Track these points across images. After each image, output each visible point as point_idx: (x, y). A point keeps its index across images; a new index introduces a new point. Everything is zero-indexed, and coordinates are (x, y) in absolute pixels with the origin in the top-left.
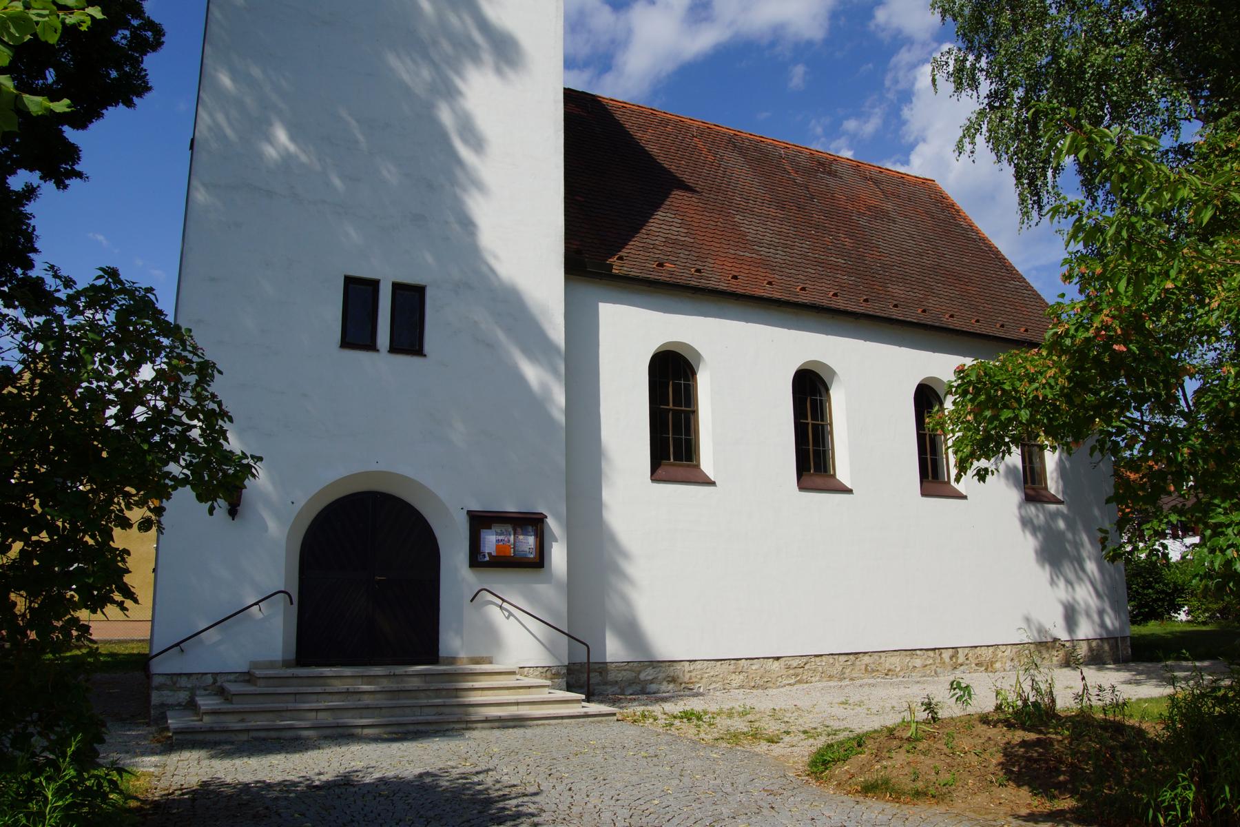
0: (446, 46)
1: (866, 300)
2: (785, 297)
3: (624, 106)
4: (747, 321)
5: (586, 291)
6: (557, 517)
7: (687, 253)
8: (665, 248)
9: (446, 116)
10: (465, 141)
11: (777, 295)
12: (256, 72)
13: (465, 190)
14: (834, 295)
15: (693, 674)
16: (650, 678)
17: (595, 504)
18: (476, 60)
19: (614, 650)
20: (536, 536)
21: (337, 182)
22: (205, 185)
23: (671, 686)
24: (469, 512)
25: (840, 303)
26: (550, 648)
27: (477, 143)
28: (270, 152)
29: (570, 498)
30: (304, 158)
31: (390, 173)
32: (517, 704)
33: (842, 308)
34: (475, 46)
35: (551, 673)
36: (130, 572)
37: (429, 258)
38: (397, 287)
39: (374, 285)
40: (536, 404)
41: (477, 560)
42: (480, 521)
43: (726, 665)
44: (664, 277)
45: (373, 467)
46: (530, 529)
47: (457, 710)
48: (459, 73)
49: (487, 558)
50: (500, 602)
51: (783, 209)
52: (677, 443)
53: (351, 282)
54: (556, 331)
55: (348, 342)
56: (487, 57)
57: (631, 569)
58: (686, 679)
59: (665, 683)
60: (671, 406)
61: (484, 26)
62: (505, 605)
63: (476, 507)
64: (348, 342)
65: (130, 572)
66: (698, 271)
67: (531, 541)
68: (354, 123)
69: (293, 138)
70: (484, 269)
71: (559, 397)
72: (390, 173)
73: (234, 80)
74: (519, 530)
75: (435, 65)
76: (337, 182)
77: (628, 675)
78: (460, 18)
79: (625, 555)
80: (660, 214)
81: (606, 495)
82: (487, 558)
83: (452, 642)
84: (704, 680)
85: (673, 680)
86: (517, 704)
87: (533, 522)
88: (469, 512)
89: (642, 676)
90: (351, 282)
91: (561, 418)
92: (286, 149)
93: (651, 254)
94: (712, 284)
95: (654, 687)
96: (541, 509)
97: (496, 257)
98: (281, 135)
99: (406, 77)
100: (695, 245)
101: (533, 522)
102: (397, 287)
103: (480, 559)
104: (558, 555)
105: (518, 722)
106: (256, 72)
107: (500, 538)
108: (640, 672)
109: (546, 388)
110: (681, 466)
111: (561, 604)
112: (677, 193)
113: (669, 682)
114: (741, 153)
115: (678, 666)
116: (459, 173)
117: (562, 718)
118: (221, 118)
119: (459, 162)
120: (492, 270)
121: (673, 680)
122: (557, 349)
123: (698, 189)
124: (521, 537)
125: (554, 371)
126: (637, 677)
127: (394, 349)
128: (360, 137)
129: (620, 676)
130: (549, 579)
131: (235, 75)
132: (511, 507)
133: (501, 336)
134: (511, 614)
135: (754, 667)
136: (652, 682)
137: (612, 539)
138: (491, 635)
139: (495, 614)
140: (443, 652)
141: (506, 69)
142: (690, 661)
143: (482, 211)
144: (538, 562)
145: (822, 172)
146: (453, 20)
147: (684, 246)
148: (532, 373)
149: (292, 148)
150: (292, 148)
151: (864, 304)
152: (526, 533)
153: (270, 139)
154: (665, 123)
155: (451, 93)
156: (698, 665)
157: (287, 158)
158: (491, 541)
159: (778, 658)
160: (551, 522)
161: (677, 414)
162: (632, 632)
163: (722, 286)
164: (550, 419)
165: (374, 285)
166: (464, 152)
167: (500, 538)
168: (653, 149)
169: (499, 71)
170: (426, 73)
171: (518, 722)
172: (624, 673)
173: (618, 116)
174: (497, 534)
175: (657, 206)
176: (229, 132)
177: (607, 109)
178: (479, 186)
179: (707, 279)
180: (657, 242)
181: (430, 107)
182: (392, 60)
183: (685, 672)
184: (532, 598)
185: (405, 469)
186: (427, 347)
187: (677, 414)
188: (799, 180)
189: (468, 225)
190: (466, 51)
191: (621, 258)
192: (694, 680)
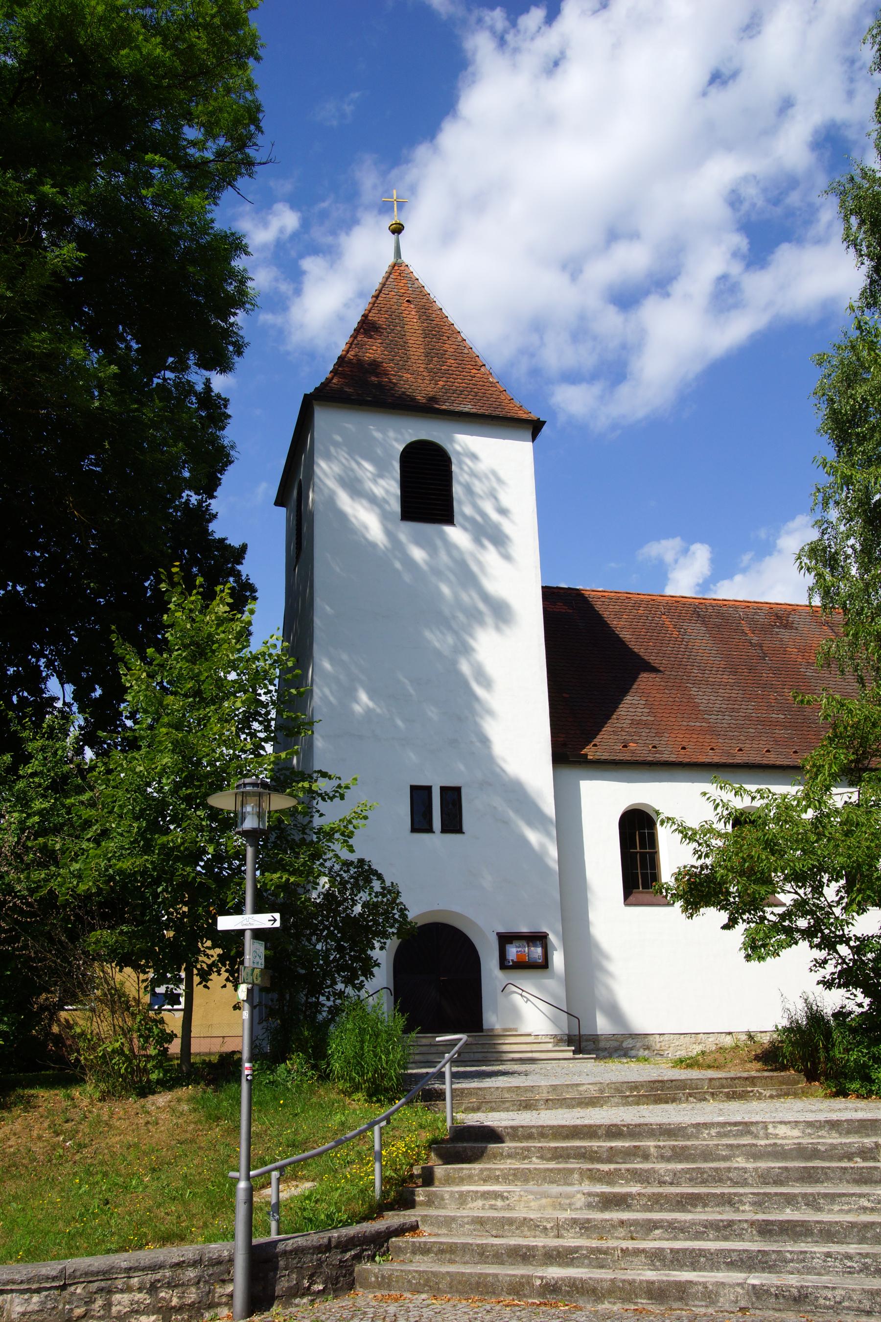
0: (461, 617)
1: (795, 752)
2: (723, 760)
3: (604, 596)
4: (693, 782)
5: (569, 773)
6: (556, 933)
7: (648, 731)
8: (630, 730)
9: (465, 667)
10: (479, 683)
11: (716, 760)
12: (345, 657)
13: (482, 718)
14: (767, 751)
15: (663, 1044)
16: (630, 1046)
17: (585, 922)
18: (482, 623)
19: (603, 1025)
20: (542, 947)
21: (400, 723)
22: (322, 737)
23: (646, 1052)
24: (498, 934)
25: (772, 759)
26: (554, 1021)
27: (486, 682)
28: (357, 708)
29: (564, 920)
30: (378, 710)
31: (432, 713)
32: (532, 1052)
33: (771, 762)
34: (480, 613)
35: (559, 1040)
36: (544, 422)
37: (462, 767)
38: (443, 789)
39: (429, 789)
40: (537, 858)
41: (504, 965)
42: (505, 939)
43: (688, 1037)
44: (627, 757)
45: (436, 908)
46: (538, 943)
47: (495, 1055)
48: (472, 636)
49: (511, 963)
50: (520, 992)
51: (735, 673)
52: (644, 876)
53: (414, 789)
54: (549, 807)
55: (416, 828)
56: (489, 619)
57: (611, 967)
58: (658, 1047)
59: (642, 1050)
60: (638, 849)
61: (486, 597)
62: (524, 994)
63: (502, 930)
64: (416, 828)
65: (544, 422)
66: (654, 747)
67: (539, 950)
68: (406, 681)
69: (371, 698)
70: (498, 770)
71: (553, 851)
72: (432, 713)
73: (332, 665)
74: (531, 944)
75: (456, 633)
76: (400, 723)
77: (616, 1044)
78: (470, 596)
79: (607, 957)
80: (628, 699)
81: (592, 916)
82: (511, 963)
83: (492, 1019)
84: (671, 1049)
85: (648, 1048)
86: (532, 1052)
87: (540, 939)
88: (498, 934)
89: (625, 1045)
90: (414, 789)
91: (555, 866)
92: (368, 707)
93: (619, 737)
94: (665, 757)
95: (633, 1053)
96: (544, 929)
97: (505, 761)
98: (363, 697)
99: (437, 645)
100: (655, 722)
101: (540, 939)
102: (443, 789)
103: (506, 964)
104: (558, 959)
105: (533, 1061)
106: (345, 657)
107: (519, 949)
108: (622, 1042)
109: (542, 846)
110: (647, 893)
111: (561, 992)
112: (644, 676)
113: (645, 1049)
114: (704, 623)
115: (651, 1038)
116: (477, 707)
117: (559, 1059)
118: (327, 691)
119: (476, 698)
120: (503, 771)
121: (648, 1048)
122: (550, 820)
123: (661, 669)
124: (532, 948)
125: (548, 834)
126: (621, 1045)
127: (444, 830)
128: (412, 691)
129: (608, 1045)
130: (552, 976)
131: (332, 660)
132: (524, 929)
133: (511, 814)
134: (528, 1000)
135: (710, 1040)
136: (632, 1049)
137: (597, 946)
138: (515, 1012)
139: (517, 999)
140: (485, 1027)
141: (501, 625)
142: (660, 1034)
143: (493, 729)
144: (544, 965)
145: (778, 627)
146: (465, 597)
147: (646, 724)
148: (533, 837)
149: (371, 704)
150: (371, 704)
151: (794, 756)
152: (535, 946)
153: (356, 700)
154: (637, 605)
155: (466, 650)
156: (666, 1037)
157: (369, 711)
158: (513, 952)
159: (730, 1033)
160: (552, 937)
161: (643, 856)
162: (614, 1012)
163: (673, 758)
164: (547, 867)
165: (429, 789)
166: (479, 691)
167: (519, 949)
168: (625, 635)
169: (498, 629)
170: (450, 640)
171: (533, 1061)
172: (611, 1042)
173: (598, 607)
174: (517, 947)
175: (625, 691)
176: (332, 699)
177: (588, 601)
178: (490, 712)
179: (661, 753)
180: (624, 725)
181: (454, 663)
182: (428, 634)
183: (657, 1045)
184: (541, 988)
185: (456, 908)
186: (465, 827)
187: (643, 856)
188: (755, 640)
189: (485, 741)
190: (475, 617)
191: (595, 745)
192: (663, 1048)
